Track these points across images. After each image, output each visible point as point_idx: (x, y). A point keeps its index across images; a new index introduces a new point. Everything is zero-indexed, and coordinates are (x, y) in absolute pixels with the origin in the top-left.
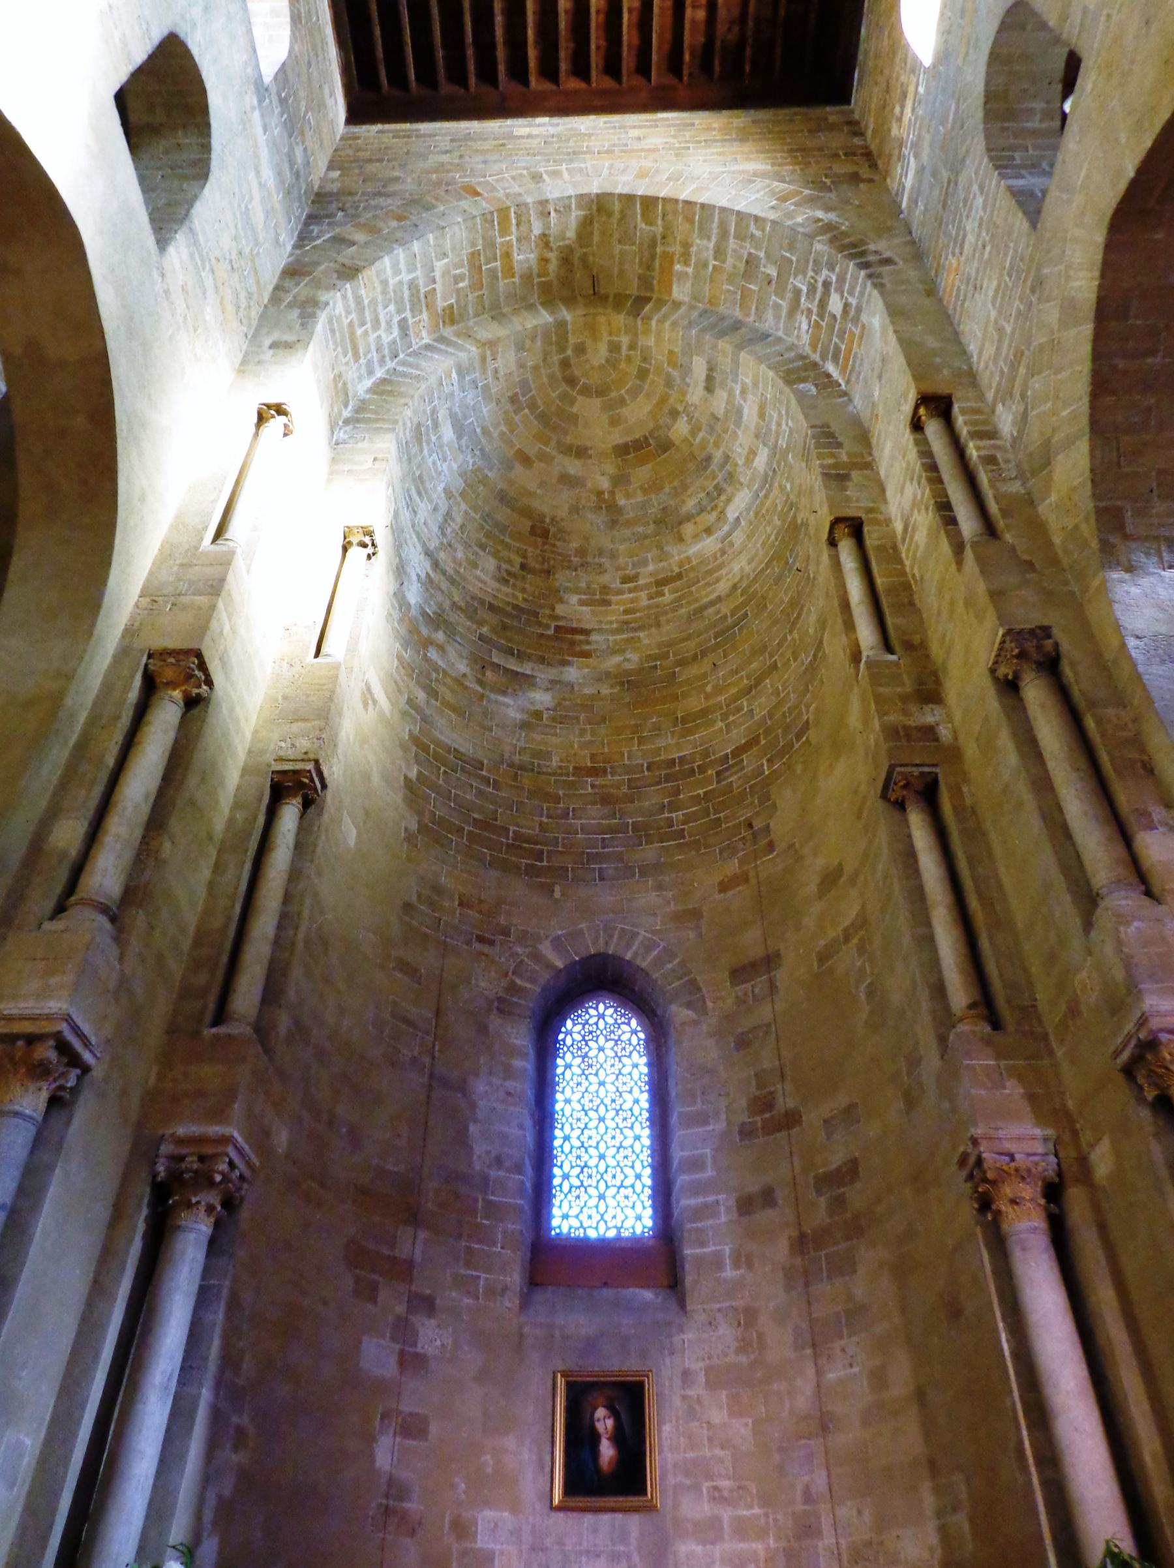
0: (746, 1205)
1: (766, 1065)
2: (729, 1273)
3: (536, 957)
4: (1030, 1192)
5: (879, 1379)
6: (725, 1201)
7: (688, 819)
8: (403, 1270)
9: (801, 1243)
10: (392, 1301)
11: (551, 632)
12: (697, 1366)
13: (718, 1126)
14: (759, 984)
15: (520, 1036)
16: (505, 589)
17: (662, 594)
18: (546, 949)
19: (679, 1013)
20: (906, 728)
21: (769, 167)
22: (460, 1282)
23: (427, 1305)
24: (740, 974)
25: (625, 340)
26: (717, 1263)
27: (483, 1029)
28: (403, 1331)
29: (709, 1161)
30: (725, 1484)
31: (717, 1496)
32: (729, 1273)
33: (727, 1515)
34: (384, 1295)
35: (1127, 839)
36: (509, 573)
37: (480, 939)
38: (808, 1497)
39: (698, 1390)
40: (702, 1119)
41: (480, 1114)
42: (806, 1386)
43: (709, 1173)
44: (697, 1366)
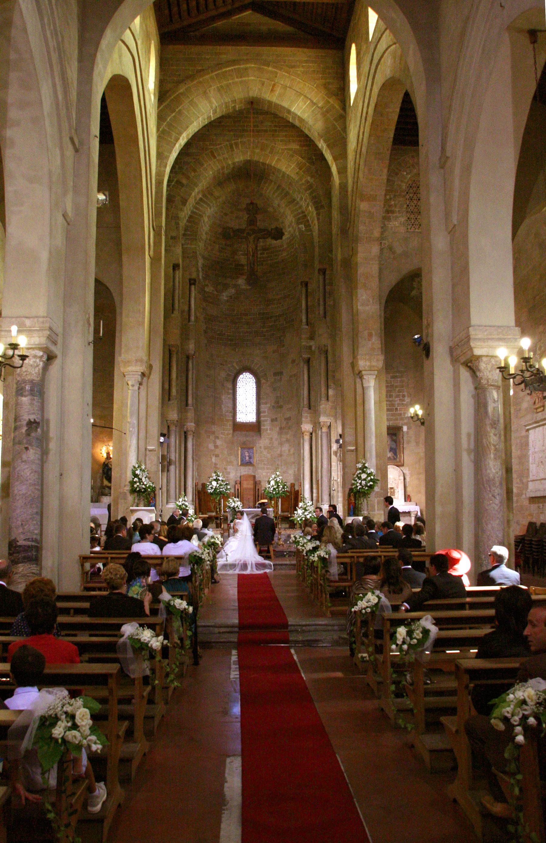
0: (272, 420)
1: (278, 395)
2: (269, 431)
3: (233, 366)
4: (308, 434)
5: (289, 451)
6: (269, 419)
7: (267, 331)
8: (214, 433)
9: (281, 428)
10: (212, 437)
11: (233, 267)
12: (262, 446)
13: (269, 405)
14: (278, 378)
15: (230, 386)
16: (222, 254)
17: (264, 254)
18: (235, 364)
19: (263, 381)
20: (307, 346)
21: (298, 147)
22: (222, 433)
23: (217, 438)
24: (275, 374)
25: (256, 190)
26: (267, 430)
27: (223, 385)
28: (215, 442)
29: (232, 664)
30: (266, 463)
31: (264, 464)
32: (269, 431)
33: (266, 467)
34: (211, 437)
35: (328, 388)
36: (222, 248)
37: (221, 364)
38: (278, 465)
39: (262, 449)
40: (266, 403)
41: (224, 402)
42: (279, 450)
43: (266, 414)
44: (262, 446)
